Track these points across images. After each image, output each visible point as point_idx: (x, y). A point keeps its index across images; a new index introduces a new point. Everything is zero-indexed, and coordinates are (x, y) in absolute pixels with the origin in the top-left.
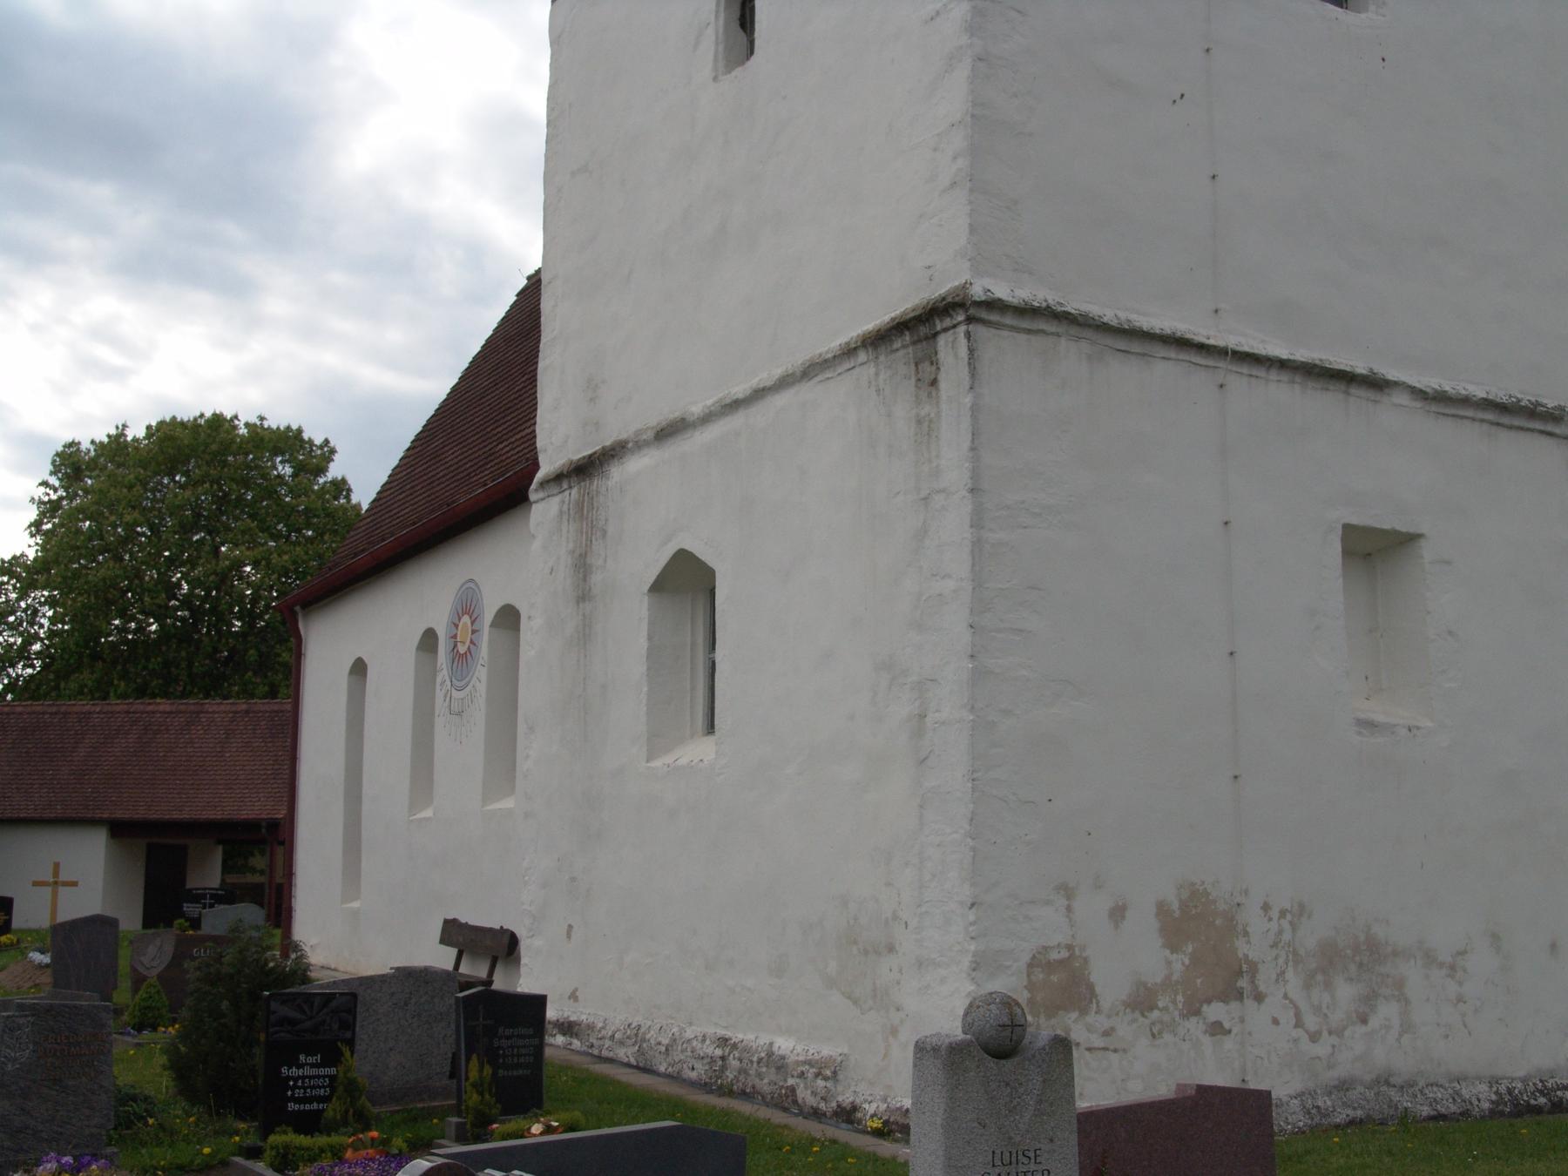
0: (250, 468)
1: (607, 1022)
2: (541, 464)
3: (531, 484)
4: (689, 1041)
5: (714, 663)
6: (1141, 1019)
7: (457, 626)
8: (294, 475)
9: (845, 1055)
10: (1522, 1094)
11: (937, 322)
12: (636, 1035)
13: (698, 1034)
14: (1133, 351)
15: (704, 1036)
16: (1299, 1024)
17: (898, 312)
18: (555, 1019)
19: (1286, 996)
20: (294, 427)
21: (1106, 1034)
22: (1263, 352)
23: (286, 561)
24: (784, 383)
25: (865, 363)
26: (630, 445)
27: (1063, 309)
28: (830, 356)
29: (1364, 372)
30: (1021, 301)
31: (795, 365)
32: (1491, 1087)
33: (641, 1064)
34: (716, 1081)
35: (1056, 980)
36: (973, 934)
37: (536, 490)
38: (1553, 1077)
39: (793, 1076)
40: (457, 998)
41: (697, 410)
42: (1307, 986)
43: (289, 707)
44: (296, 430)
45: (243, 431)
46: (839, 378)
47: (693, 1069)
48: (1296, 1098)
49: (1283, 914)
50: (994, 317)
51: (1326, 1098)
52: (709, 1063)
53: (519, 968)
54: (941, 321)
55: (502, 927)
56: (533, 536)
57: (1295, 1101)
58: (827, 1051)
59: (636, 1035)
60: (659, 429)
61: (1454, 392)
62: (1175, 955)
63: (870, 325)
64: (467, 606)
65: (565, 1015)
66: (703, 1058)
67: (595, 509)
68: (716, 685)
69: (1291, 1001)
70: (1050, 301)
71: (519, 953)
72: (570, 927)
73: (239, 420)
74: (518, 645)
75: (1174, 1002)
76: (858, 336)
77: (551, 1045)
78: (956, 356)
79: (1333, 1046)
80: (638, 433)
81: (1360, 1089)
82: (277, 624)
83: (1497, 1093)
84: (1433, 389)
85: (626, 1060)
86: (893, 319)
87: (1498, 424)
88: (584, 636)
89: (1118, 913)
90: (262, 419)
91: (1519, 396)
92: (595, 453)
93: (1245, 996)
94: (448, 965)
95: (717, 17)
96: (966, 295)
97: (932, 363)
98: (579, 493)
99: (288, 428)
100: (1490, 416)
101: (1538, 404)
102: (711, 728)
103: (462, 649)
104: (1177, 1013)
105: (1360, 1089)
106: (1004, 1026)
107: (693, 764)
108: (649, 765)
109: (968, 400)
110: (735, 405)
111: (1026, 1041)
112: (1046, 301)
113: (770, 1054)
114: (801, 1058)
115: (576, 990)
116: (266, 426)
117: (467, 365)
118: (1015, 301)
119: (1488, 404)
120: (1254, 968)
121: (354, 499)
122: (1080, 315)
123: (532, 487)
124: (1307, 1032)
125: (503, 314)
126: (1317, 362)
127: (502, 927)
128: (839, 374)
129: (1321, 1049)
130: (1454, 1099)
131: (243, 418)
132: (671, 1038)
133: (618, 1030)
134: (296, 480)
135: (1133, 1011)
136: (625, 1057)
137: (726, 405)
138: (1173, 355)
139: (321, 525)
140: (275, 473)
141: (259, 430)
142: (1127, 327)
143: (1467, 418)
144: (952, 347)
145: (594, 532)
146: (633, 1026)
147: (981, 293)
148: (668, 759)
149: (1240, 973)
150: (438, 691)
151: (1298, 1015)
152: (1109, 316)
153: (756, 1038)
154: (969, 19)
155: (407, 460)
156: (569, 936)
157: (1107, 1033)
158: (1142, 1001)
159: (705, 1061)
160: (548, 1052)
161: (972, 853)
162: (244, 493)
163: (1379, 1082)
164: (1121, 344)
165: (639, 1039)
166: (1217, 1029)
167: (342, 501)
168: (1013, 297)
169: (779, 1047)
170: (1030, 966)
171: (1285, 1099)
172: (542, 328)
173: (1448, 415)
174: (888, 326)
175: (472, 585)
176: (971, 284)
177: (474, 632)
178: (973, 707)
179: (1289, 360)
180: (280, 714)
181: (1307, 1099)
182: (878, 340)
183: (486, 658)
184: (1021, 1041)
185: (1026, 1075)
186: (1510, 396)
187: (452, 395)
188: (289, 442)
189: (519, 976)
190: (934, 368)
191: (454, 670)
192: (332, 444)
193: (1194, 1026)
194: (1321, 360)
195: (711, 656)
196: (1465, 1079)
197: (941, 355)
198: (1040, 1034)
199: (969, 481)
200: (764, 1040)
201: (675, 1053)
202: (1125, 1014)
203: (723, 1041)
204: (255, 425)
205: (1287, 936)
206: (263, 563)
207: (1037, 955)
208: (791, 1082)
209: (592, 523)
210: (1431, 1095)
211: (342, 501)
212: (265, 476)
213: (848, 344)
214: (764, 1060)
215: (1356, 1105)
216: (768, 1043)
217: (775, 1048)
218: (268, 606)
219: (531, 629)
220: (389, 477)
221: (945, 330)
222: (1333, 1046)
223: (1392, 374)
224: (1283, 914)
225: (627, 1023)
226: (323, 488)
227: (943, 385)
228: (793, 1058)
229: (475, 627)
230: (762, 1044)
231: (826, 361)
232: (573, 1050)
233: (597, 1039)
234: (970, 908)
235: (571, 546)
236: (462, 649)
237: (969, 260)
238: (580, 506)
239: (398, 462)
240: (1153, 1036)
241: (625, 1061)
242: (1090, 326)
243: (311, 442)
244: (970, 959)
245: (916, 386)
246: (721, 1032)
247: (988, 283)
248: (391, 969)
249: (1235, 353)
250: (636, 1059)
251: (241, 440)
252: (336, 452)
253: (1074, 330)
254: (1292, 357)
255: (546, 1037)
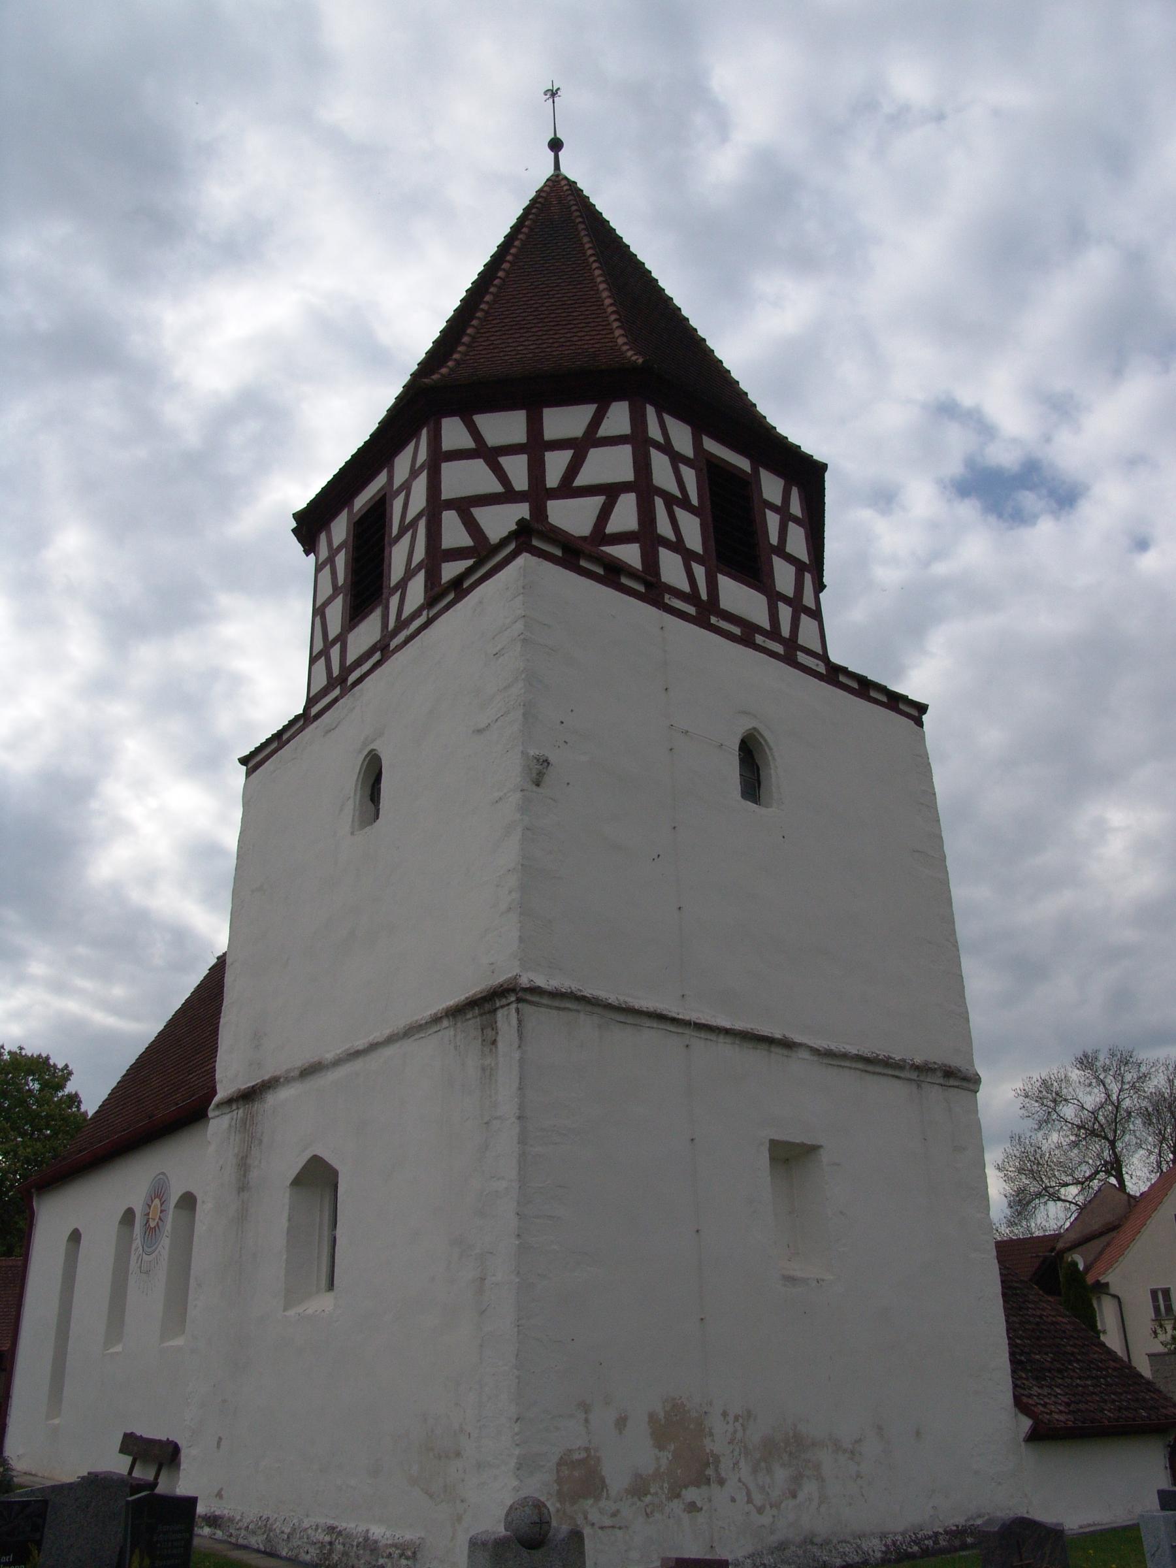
0: (8, 1083)
1: (244, 1515)
2: (218, 1091)
3: (209, 1106)
4: (306, 1529)
5: (335, 1238)
6: (639, 1503)
7: (150, 1206)
8: (41, 1090)
9: (423, 1539)
10: (902, 1545)
11: (497, 1001)
12: (266, 1526)
13: (312, 1524)
14: (628, 1022)
15: (317, 1526)
16: (750, 1501)
17: (470, 993)
18: (204, 1513)
19: (740, 1480)
20: (44, 1055)
21: (614, 1515)
22: (715, 1024)
23: (29, 1153)
24: (390, 1040)
25: (447, 1027)
26: (282, 1080)
27: (582, 994)
28: (423, 1022)
29: (779, 1037)
30: (554, 988)
31: (399, 1027)
32: (881, 1540)
33: (268, 1550)
34: (325, 1563)
35: (577, 1475)
36: (517, 1442)
37: (213, 1110)
38: (922, 1530)
39: (383, 1557)
40: (127, 1501)
41: (329, 1056)
42: (755, 1471)
43: (20, 1263)
44: (46, 1057)
45: (6, 1057)
46: (430, 1037)
47: (308, 1552)
48: (749, 1558)
49: (736, 1418)
50: (535, 999)
51: (770, 1557)
52: (320, 1548)
53: (179, 1474)
54: (500, 1000)
55: (168, 1439)
56: (209, 1142)
57: (748, 1561)
58: (409, 1535)
59: (266, 1526)
60: (303, 1069)
61: (837, 1050)
62: (662, 1453)
63: (451, 1002)
64: (158, 1192)
65: (212, 1510)
66: (315, 1543)
67: (255, 1125)
68: (336, 1261)
69: (744, 1484)
70: (573, 988)
71: (180, 1459)
72: (220, 1439)
73: (4, 1049)
74: (194, 1221)
75: (662, 1488)
76: (443, 1009)
77: (199, 1535)
78: (509, 1024)
79: (774, 1516)
80: (288, 1071)
81: (793, 1548)
82: (18, 1199)
83: (886, 1545)
84: (823, 1047)
85: (256, 1546)
86: (467, 998)
87: (866, 1071)
88: (242, 1217)
89: (621, 1422)
90: (21, 1048)
91: (878, 1053)
92: (257, 1084)
93: (711, 1482)
94: (124, 1471)
95: (355, 794)
96: (516, 984)
97: (493, 1029)
98: (244, 1113)
99: (40, 1056)
100: (860, 1066)
101: (890, 1058)
102: (331, 1286)
103: (152, 1224)
104: (664, 1496)
105: (793, 1548)
106: (535, 1523)
107: (318, 1313)
108: (286, 1313)
109: (517, 1055)
110: (357, 1054)
111: (551, 1534)
112: (570, 988)
113: (366, 1539)
114: (390, 1542)
115: (222, 1489)
116: (23, 1054)
117: (171, 1017)
118: (549, 988)
119: (859, 1058)
120: (717, 1460)
121: (83, 1108)
122: (593, 998)
123: (210, 1108)
124: (754, 1506)
125: (199, 983)
126: (749, 1030)
127: (168, 1439)
128: (429, 1035)
129: (766, 1520)
130: (857, 1552)
131: (7, 1048)
132: (292, 1528)
133: (252, 1522)
134: (42, 1093)
135: (633, 1497)
136: (255, 1544)
137: (351, 1054)
138: (655, 1025)
139: (57, 1128)
140: (27, 1088)
141: (18, 1057)
142: (624, 1006)
143: (846, 1067)
144: (506, 1018)
145: (253, 1141)
146: (264, 1518)
147: (527, 982)
148: (300, 1309)
149: (707, 1464)
150: (132, 1255)
151: (749, 1494)
152: (612, 999)
153: (357, 1526)
154: (520, 803)
155: (128, 1078)
156: (219, 1446)
157: (614, 1515)
158: (639, 1489)
159: (317, 1546)
160: (196, 1541)
161: (517, 1380)
162: (3, 1102)
163: (806, 1542)
164: (621, 1018)
165: (267, 1529)
166: (692, 1507)
167: (73, 1110)
168: (548, 985)
169: (374, 1534)
170: (559, 1464)
171: (741, 1559)
172: (225, 995)
173: (834, 1065)
174: (464, 1002)
175: (161, 1176)
176: (520, 976)
177: (162, 1211)
178: (518, 1273)
179: (731, 1029)
180: (13, 1269)
181: (757, 1558)
182: (456, 1012)
183: (169, 1231)
184: (547, 1535)
185: (551, 1562)
186: (872, 1053)
187: (158, 1038)
188: (39, 1066)
189: (179, 1478)
190: (494, 1033)
191: (146, 1238)
192: (70, 1068)
193: (676, 1506)
194: (752, 1029)
195: (333, 1233)
196: (864, 1535)
197: (499, 1024)
198: (561, 1528)
199: (518, 1111)
200: (362, 1528)
201: (294, 1540)
202: (627, 1499)
203: (331, 1529)
204: (16, 1053)
205: (739, 1435)
206: (12, 1154)
207: (563, 1456)
208: (381, 1561)
209: (252, 1134)
210: (842, 1550)
211: (73, 1110)
212: (19, 1090)
213: (436, 1014)
214: (361, 1544)
215: (791, 1561)
216: (365, 1530)
217: (370, 1535)
218: (12, 1186)
219: (204, 1208)
220: (109, 1095)
221: (502, 1007)
222: (774, 1516)
223: (797, 1038)
224: (736, 1418)
225: (259, 1515)
226: (61, 1099)
227: (500, 1044)
228: (384, 1542)
229: (163, 1208)
230: (360, 1531)
231: (421, 1026)
232: (216, 1539)
233: (236, 1529)
234: (516, 1422)
235: (236, 1150)
236: (152, 1224)
237: (519, 960)
238: (244, 1122)
239: (107, 1096)
240: (647, 1514)
241: (256, 1548)
242: (599, 1005)
243: (55, 1066)
244: (516, 1461)
245: (482, 1045)
246: (331, 1522)
247: (532, 975)
248: (78, 1478)
249: (696, 1024)
250: (264, 1546)
251: (5, 1064)
252: (73, 1074)
253: (589, 1008)
254: (733, 1027)
255: (196, 1529)
